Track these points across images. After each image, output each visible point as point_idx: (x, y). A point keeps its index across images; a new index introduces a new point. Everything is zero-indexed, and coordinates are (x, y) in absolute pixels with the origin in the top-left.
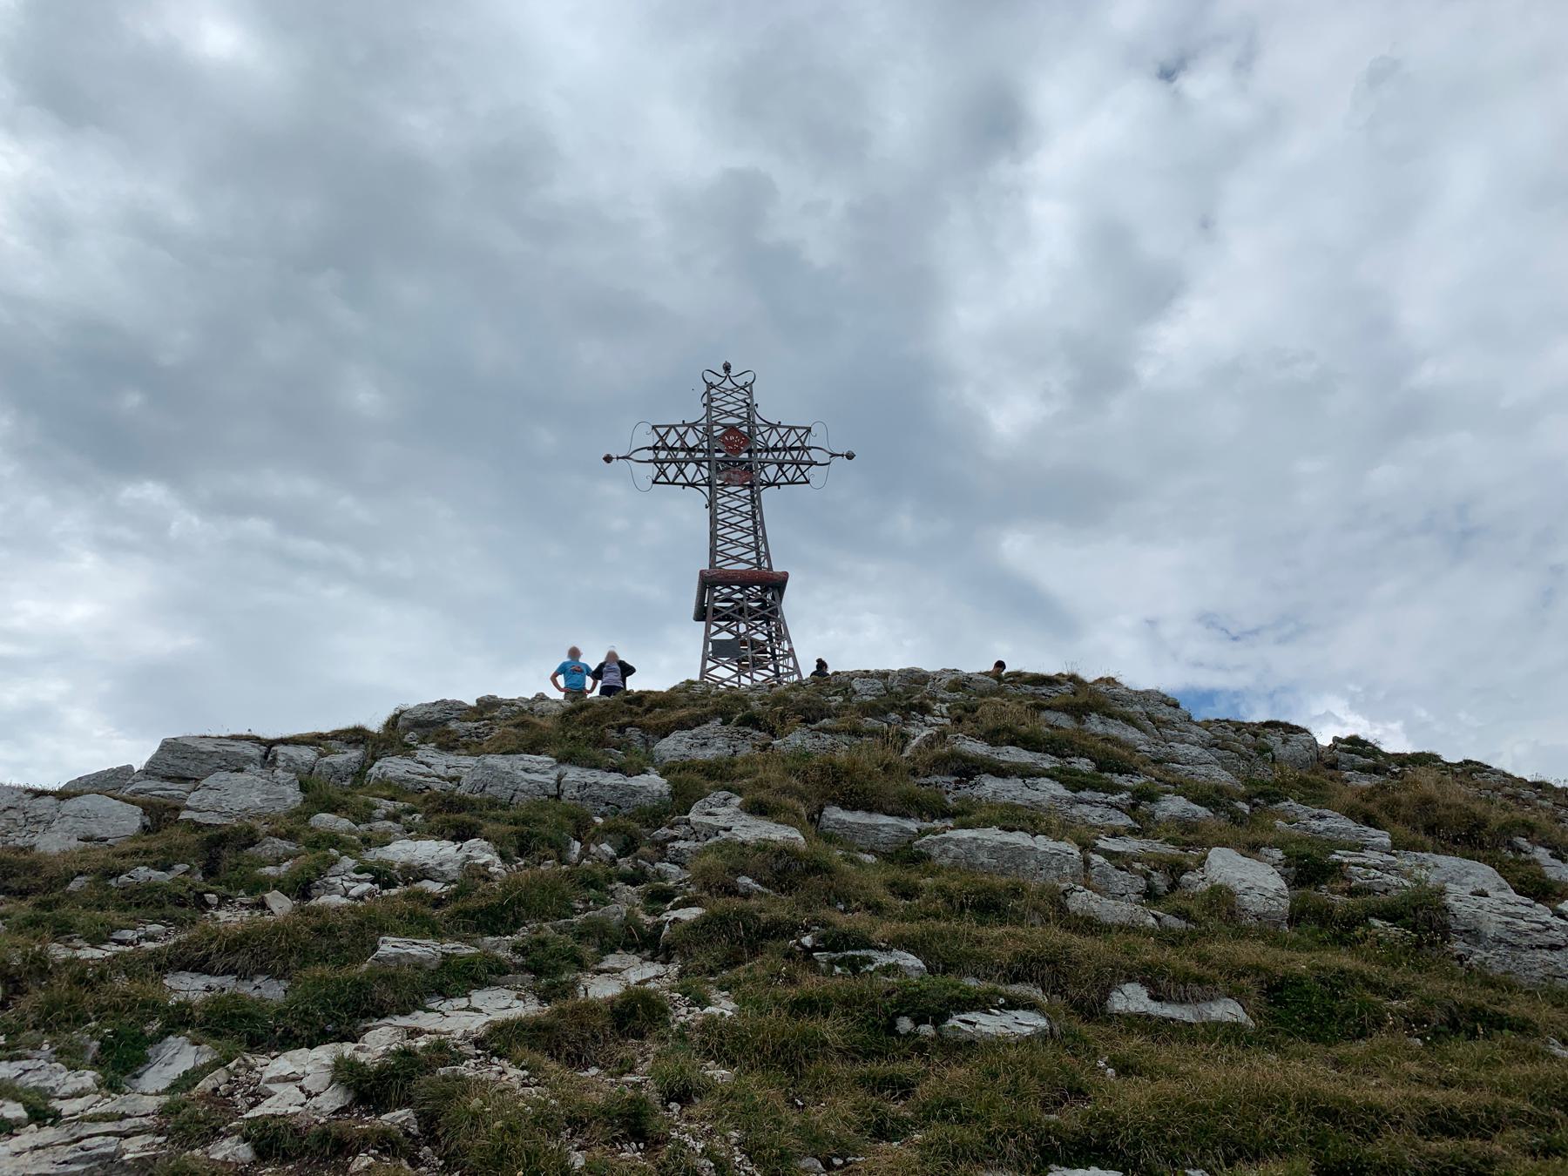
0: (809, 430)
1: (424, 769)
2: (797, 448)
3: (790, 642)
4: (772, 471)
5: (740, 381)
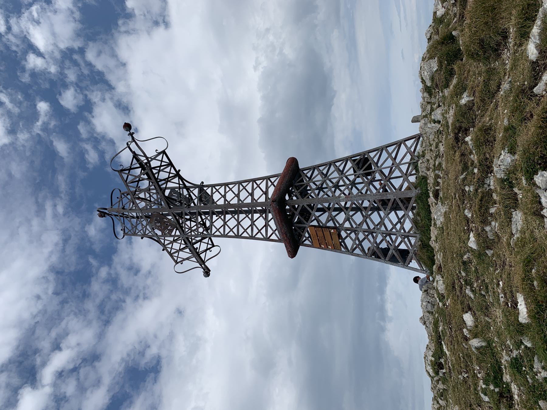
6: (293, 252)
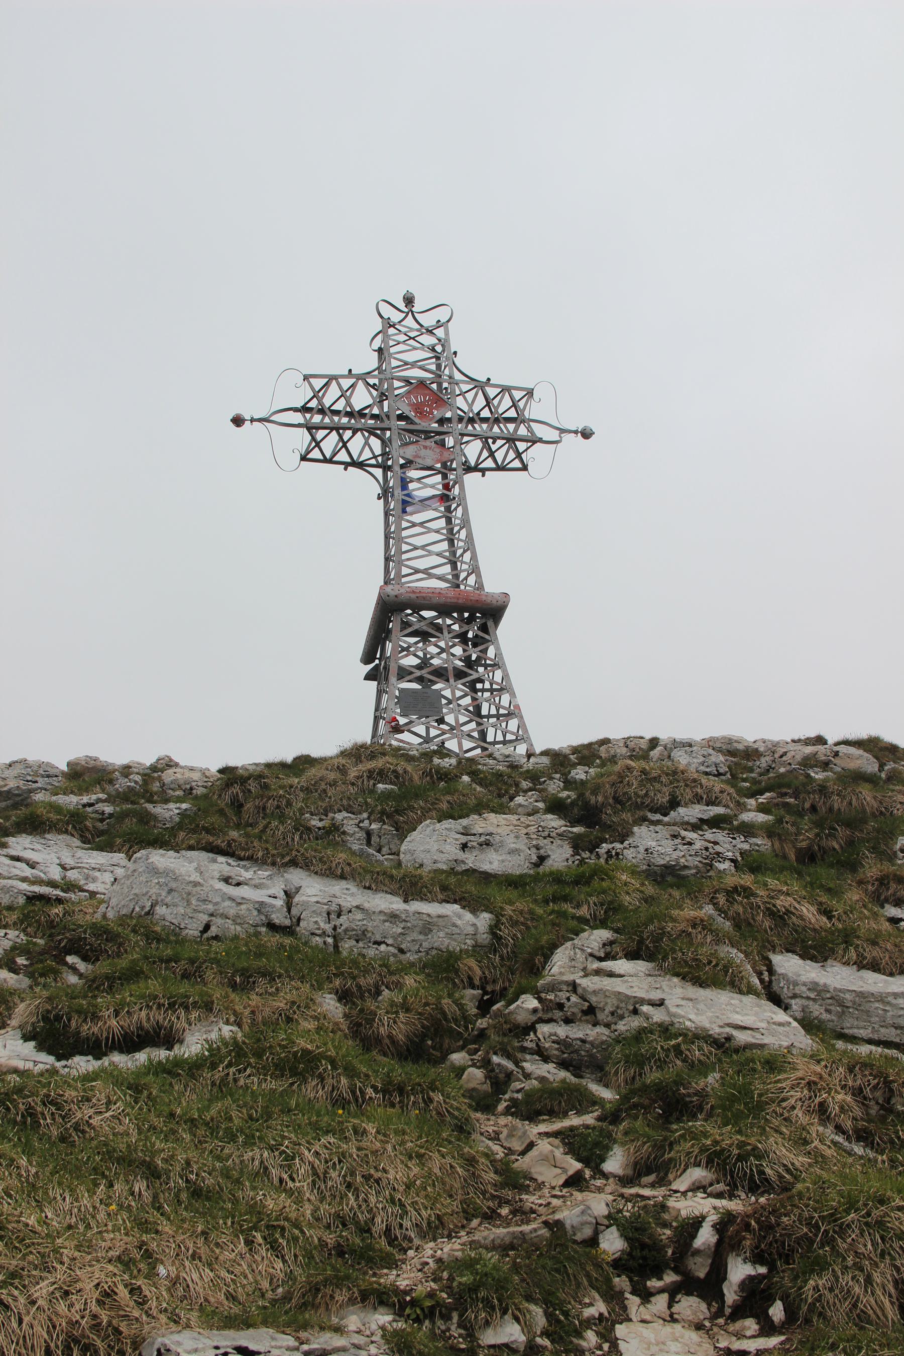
0: (530, 393)
1: (28, 872)
2: (485, 420)
3: (513, 695)
4: (473, 450)
5: (428, 320)
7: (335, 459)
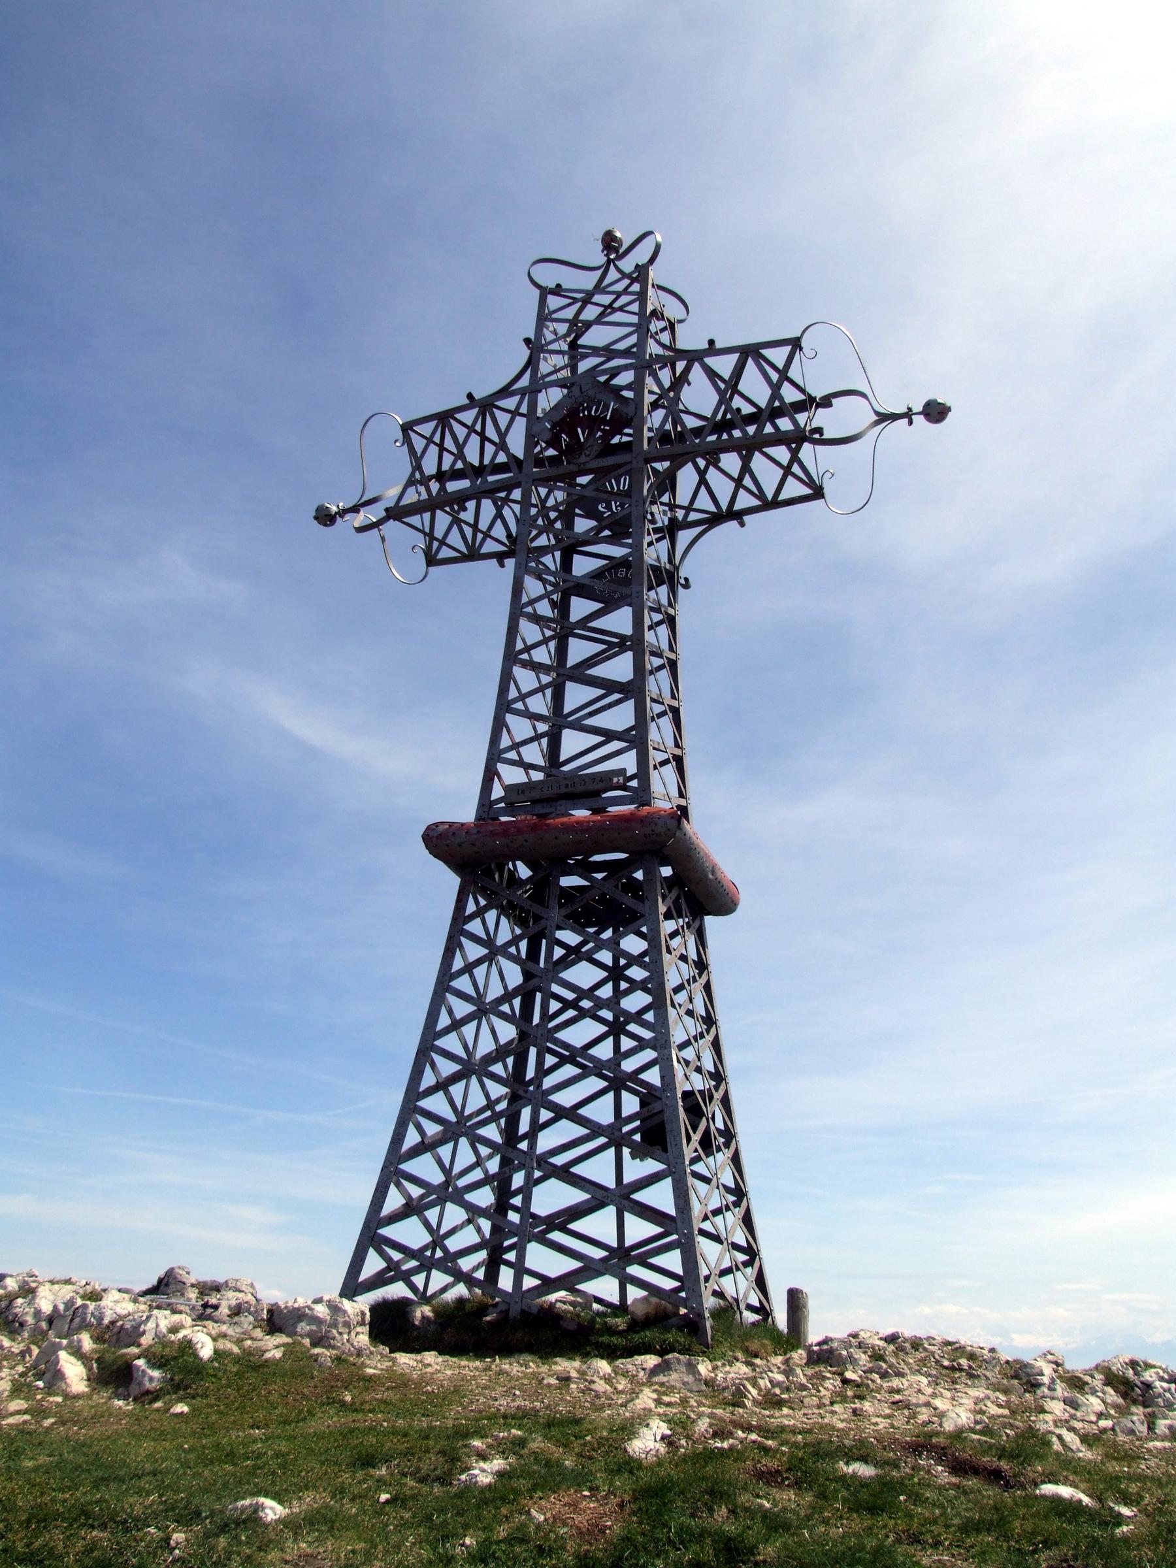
6: (441, 841)
7: (782, 497)
